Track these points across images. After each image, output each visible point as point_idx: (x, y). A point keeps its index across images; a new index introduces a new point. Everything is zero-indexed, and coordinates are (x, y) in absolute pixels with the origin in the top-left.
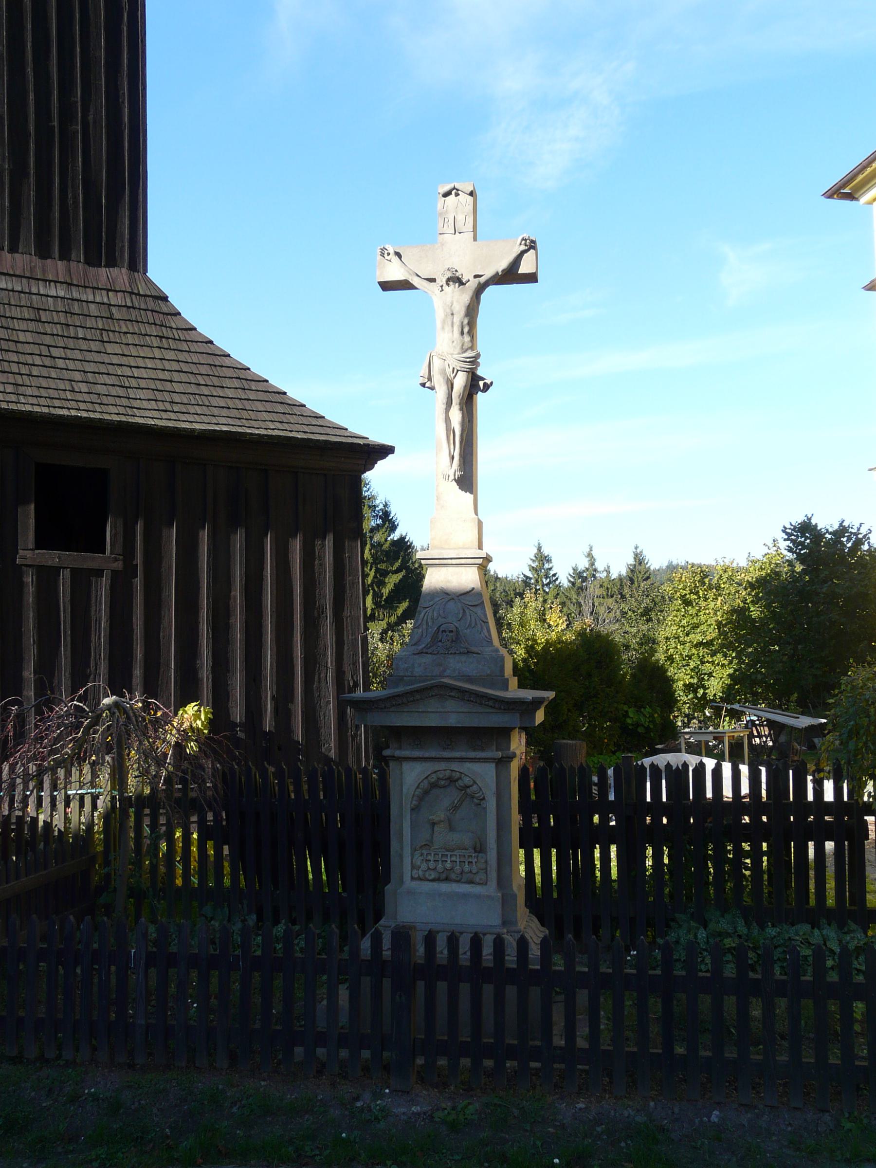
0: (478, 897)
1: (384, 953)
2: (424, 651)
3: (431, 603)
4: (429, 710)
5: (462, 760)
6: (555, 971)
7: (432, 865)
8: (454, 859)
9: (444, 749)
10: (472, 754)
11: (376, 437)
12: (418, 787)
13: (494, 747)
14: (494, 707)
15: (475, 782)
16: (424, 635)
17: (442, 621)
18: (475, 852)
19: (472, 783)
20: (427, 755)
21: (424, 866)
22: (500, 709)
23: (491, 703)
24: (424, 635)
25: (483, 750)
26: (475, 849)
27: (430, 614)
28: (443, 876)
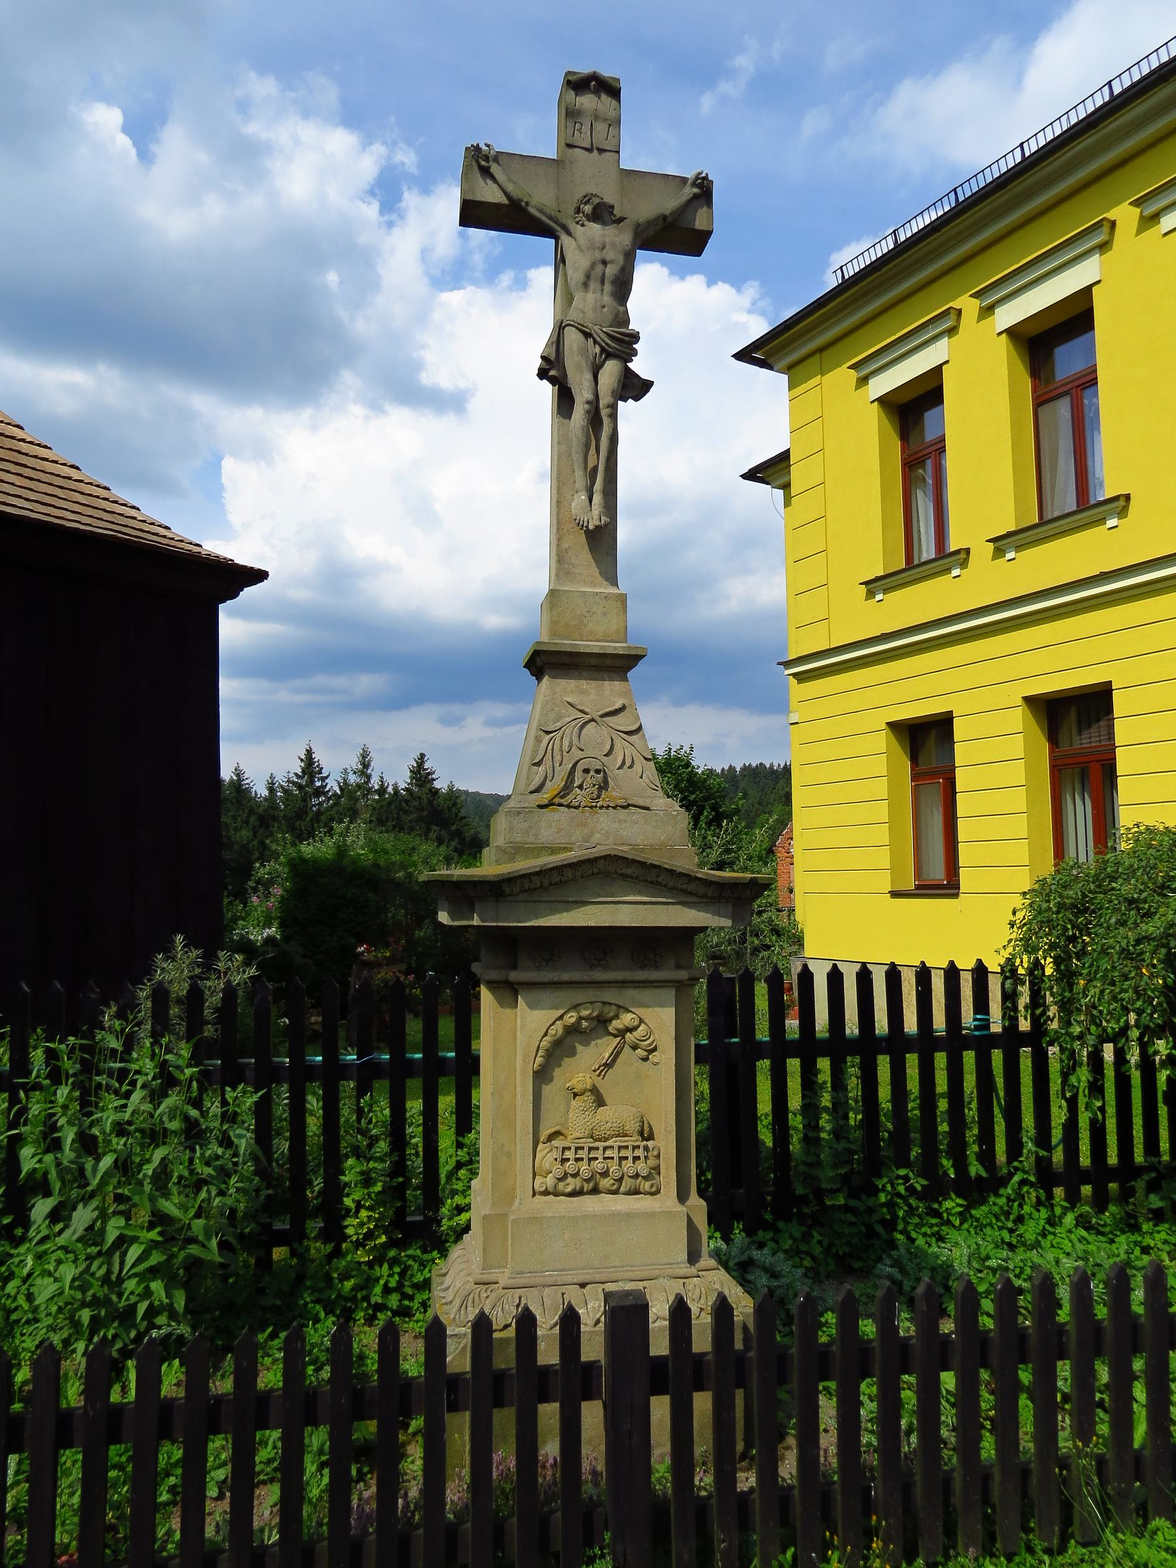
0: (649, 1215)
1: (496, 1335)
2: (557, 800)
3: (558, 725)
4: (586, 899)
5: (623, 984)
6: (410, 1222)
7: (570, 1167)
8: (609, 1153)
9: (592, 967)
10: (641, 975)
11: (241, 554)
12: (546, 1034)
13: (673, 963)
14: (695, 895)
15: (641, 1021)
16: (549, 777)
17: (579, 755)
18: (644, 1139)
19: (636, 1023)
20: (566, 976)
21: (558, 1170)
22: (705, 896)
23: (691, 887)
24: (549, 777)
25: (657, 967)
26: (641, 1133)
27: (557, 742)
28: (587, 1187)
